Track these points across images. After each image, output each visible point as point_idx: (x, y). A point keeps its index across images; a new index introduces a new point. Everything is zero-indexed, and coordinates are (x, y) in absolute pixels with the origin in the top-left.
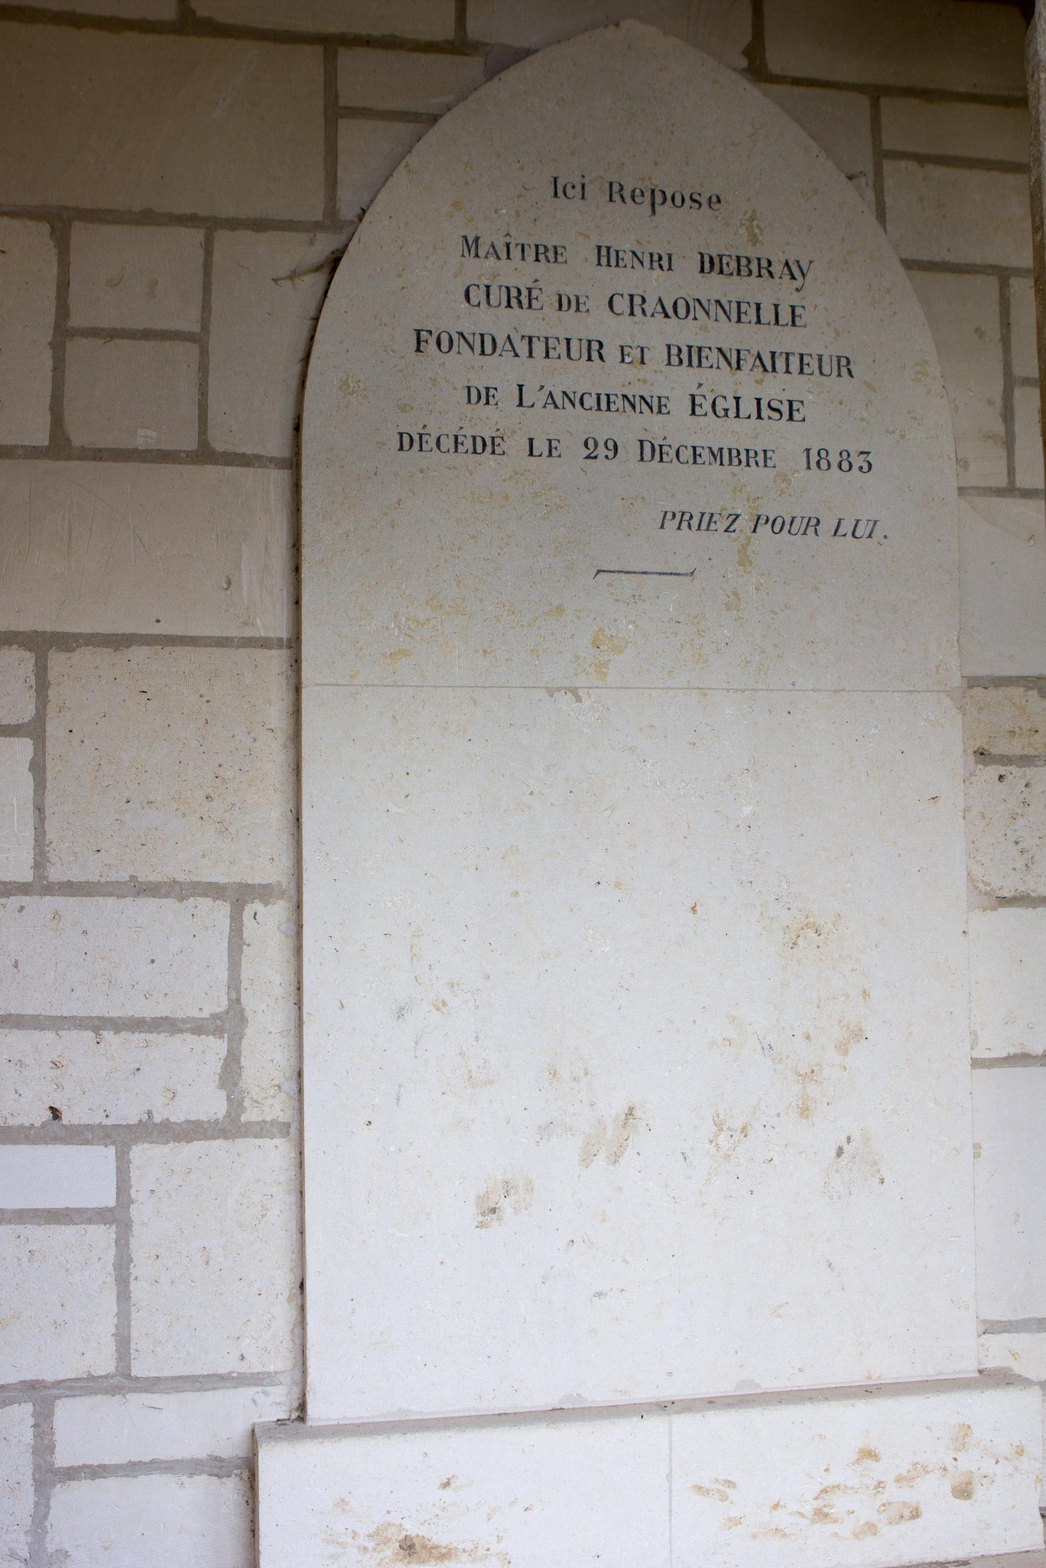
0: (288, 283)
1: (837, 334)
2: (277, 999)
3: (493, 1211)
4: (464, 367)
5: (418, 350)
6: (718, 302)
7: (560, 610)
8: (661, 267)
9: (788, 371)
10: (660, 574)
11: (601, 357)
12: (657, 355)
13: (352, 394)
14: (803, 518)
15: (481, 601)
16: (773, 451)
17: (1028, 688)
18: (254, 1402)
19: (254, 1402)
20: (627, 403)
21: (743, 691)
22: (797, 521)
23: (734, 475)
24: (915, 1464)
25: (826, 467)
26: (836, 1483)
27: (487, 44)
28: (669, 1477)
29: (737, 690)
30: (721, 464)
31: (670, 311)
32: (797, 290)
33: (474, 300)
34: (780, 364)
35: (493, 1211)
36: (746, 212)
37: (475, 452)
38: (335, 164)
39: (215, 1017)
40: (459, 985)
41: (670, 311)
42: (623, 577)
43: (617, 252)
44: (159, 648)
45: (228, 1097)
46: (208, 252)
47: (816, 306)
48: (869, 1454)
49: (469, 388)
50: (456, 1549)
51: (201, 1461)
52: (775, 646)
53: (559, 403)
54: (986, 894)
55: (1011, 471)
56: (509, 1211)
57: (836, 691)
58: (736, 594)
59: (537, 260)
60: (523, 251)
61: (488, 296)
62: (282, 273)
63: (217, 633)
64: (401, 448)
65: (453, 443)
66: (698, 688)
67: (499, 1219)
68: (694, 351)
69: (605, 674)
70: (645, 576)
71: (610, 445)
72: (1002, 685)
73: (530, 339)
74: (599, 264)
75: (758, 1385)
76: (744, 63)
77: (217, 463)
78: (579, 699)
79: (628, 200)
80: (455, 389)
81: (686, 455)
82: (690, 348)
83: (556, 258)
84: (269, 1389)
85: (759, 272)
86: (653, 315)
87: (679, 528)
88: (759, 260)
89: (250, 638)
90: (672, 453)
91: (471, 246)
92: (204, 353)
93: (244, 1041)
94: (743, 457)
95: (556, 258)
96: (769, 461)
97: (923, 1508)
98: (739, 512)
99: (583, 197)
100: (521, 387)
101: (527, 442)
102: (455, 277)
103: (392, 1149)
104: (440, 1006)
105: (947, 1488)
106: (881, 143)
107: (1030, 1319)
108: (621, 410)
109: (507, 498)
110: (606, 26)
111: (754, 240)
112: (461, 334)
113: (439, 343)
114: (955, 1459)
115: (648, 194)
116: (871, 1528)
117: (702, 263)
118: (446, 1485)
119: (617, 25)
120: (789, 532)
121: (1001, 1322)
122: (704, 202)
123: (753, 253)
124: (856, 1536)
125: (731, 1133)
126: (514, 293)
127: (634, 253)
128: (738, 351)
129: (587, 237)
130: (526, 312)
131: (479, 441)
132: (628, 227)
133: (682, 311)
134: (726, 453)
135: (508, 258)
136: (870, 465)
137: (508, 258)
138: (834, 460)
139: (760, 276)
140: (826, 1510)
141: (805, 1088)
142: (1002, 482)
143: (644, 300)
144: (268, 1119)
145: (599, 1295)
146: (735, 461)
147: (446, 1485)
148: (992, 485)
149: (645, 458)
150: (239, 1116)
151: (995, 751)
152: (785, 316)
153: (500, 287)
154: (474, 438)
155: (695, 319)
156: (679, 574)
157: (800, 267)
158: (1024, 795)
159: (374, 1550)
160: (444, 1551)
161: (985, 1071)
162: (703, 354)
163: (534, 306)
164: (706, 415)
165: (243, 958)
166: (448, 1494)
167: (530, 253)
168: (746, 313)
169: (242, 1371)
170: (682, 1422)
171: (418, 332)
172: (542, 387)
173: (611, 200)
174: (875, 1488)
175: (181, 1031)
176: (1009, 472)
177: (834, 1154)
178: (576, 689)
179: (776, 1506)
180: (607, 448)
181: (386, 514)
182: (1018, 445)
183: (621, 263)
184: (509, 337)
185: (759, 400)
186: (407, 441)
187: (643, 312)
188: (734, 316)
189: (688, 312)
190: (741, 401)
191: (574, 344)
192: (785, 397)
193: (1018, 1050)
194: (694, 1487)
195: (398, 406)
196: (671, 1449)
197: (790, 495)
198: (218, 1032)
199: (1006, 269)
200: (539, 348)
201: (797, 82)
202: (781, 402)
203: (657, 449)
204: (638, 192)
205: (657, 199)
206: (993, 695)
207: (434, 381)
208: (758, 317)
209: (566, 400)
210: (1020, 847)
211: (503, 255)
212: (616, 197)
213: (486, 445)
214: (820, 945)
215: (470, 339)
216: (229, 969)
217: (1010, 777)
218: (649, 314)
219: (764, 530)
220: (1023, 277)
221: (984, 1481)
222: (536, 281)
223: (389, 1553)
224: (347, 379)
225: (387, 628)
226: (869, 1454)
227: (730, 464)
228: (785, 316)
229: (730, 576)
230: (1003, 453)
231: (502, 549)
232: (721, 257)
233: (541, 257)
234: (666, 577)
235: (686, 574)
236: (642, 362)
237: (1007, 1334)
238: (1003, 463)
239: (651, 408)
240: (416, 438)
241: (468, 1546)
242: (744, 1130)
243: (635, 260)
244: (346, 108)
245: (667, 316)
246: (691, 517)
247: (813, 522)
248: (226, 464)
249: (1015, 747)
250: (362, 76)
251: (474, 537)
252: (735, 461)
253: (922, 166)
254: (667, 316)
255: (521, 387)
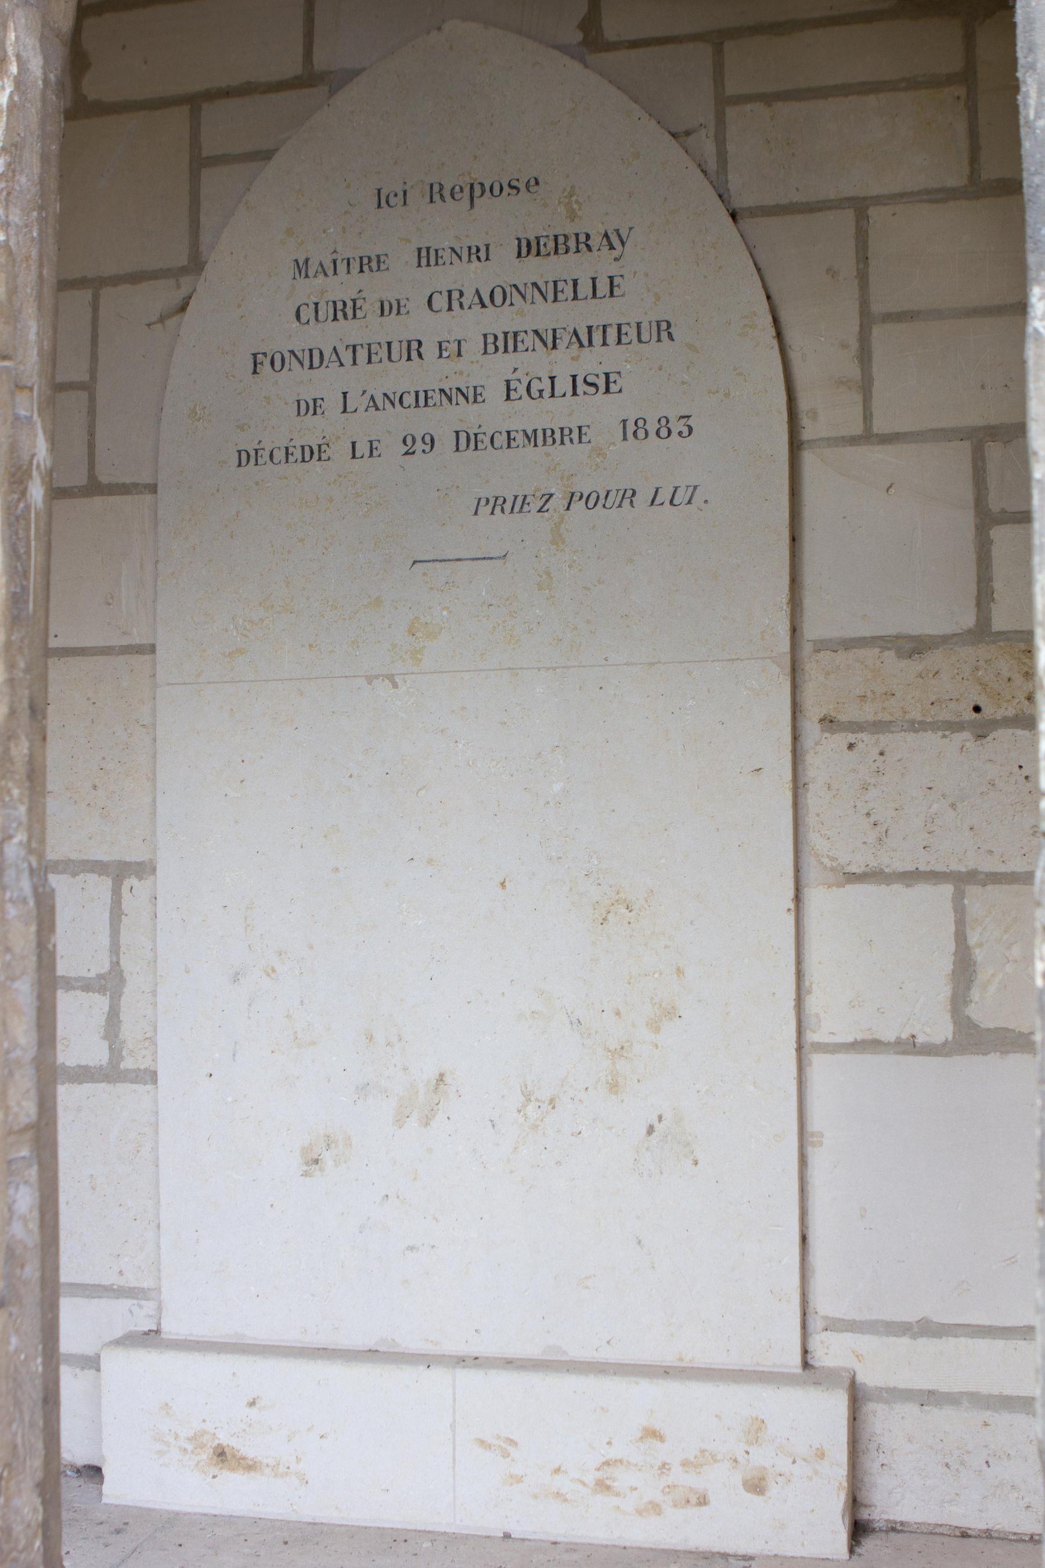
0: (159, 326)
1: (658, 298)
2: (149, 963)
3: (316, 1161)
4: (298, 383)
5: (255, 372)
6: (535, 285)
7: (378, 602)
8: (479, 258)
9: (604, 344)
10: (473, 559)
11: (420, 355)
12: (473, 346)
13: (199, 420)
14: (618, 491)
15: (308, 598)
16: (588, 426)
17: (884, 649)
18: (131, 1312)
19: (131, 1312)
20: (444, 397)
21: (554, 669)
22: (612, 495)
23: (548, 455)
24: (703, 1451)
25: (644, 436)
26: (619, 1457)
27: (331, 72)
28: (453, 1426)
29: (548, 669)
30: (536, 445)
31: (487, 300)
32: (616, 259)
33: (304, 319)
34: (597, 337)
35: (316, 1161)
36: (565, 189)
37: (303, 461)
38: (198, 211)
39: (100, 977)
40: (286, 953)
41: (487, 300)
42: (438, 565)
43: (437, 251)
44: (56, 659)
45: (110, 1047)
46: (95, 309)
47: (635, 273)
48: (652, 1434)
49: (298, 402)
50: (260, 1462)
51: (90, 1357)
52: (588, 622)
53: (380, 405)
54: (832, 869)
55: (868, 417)
56: (330, 1163)
57: (651, 664)
58: (548, 574)
59: (362, 271)
60: (348, 264)
61: (317, 312)
62: (154, 319)
63: (101, 644)
64: (240, 465)
65: (284, 455)
66: (509, 668)
67: (322, 1170)
68: (510, 337)
69: (420, 660)
70: (459, 563)
71: (428, 439)
72: (854, 647)
73: (354, 347)
74: (419, 265)
75: (565, 1352)
76: (579, 36)
77: (102, 494)
78: (395, 685)
79: (448, 198)
80: (286, 404)
81: (501, 440)
82: (506, 334)
83: (379, 267)
84: (143, 1302)
85: (577, 248)
86: (470, 308)
87: (492, 513)
88: (577, 235)
89: (127, 646)
90: (487, 440)
91: (302, 268)
92: (92, 399)
93: (123, 998)
94: (557, 436)
95: (379, 267)
96: (583, 437)
97: (711, 1497)
98: (553, 491)
99: (405, 203)
100: (345, 394)
101: (350, 446)
102: (287, 299)
103: (230, 1099)
104: (271, 972)
105: (737, 1479)
106: (724, 89)
107: (877, 1321)
108: (438, 404)
109: (331, 500)
110: (429, 33)
111: (572, 216)
112: (292, 352)
113: (272, 363)
114: (747, 1453)
115: (467, 190)
116: (655, 1508)
117: (519, 247)
118: (252, 1404)
119: (439, 29)
120: (604, 506)
121: (843, 1320)
122: (522, 186)
123: (570, 229)
124: (639, 1512)
125: (538, 1104)
126: (340, 306)
127: (453, 249)
128: (554, 331)
129: (408, 241)
130: (350, 322)
131: (307, 450)
132: (446, 225)
133: (498, 299)
134: (540, 434)
135: (335, 273)
136: (691, 430)
137: (335, 273)
138: (652, 428)
139: (578, 251)
140: (608, 1482)
141: (614, 1063)
142: (857, 429)
143: (461, 294)
144: (142, 1067)
145: (411, 1248)
146: (550, 440)
147: (252, 1404)
148: (844, 434)
149: (461, 449)
150: (119, 1064)
151: (843, 718)
152: (603, 288)
153: (327, 303)
154: (303, 447)
155: (512, 304)
156: (491, 558)
157: (619, 236)
158: (877, 764)
159: (193, 1452)
160: (250, 1463)
161: (828, 1056)
162: (519, 339)
163: (358, 316)
164: (520, 398)
165: (122, 927)
166: (253, 1412)
167: (355, 266)
168: (562, 291)
169: (122, 1284)
170: (466, 1377)
171: (255, 355)
172: (364, 392)
173: (431, 202)
174: (659, 1468)
175: (74, 988)
176: (865, 418)
177: (644, 1131)
178: (393, 675)
179: (557, 1471)
180: (424, 443)
181: (226, 526)
182: (877, 385)
183: (440, 261)
184: (335, 349)
185: (574, 377)
186: (245, 458)
187: (461, 306)
188: (550, 296)
189: (505, 299)
190: (556, 380)
191: (395, 347)
192: (601, 370)
193: (868, 1036)
194: (476, 1439)
195: (238, 427)
196: (454, 1400)
197: (605, 469)
198: (102, 990)
199: (865, 199)
200: (362, 355)
201: (634, 44)
202: (597, 376)
203: (472, 437)
204: (457, 189)
205: (474, 192)
206: (842, 657)
207: (267, 399)
208: (575, 292)
209: (387, 401)
210: (872, 819)
211: (330, 272)
212: (436, 197)
213: (313, 453)
214: (632, 921)
215: (300, 355)
216: (111, 936)
217: (861, 745)
218: (466, 307)
219: (578, 506)
220: (885, 204)
221: (779, 1479)
222: (360, 291)
223: (204, 1457)
224: (195, 407)
225: (226, 630)
226: (652, 1434)
227: (545, 444)
228: (603, 288)
229: (543, 555)
230: (858, 398)
231: (326, 548)
232: (538, 239)
233: (366, 268)
234: (479, 562)
235: (499, 558)
236: (459, 354)
237: (850, 1334)
238: (859, 408)
239: (467, 399)
240: (252, 454)
241: (272, 1462)
242: (552, 1101)
243: (454, 255)
244: (208, 158)
245: (483, 306)
246: (505, 501)
247: (629, 493)
248: (110, 494)
249: (868, 713)
250: (225, 127)
251: (301, 540)
252: (550, 440)
253: (770, 105)
254: (483, 306)
255: (345, 394)
